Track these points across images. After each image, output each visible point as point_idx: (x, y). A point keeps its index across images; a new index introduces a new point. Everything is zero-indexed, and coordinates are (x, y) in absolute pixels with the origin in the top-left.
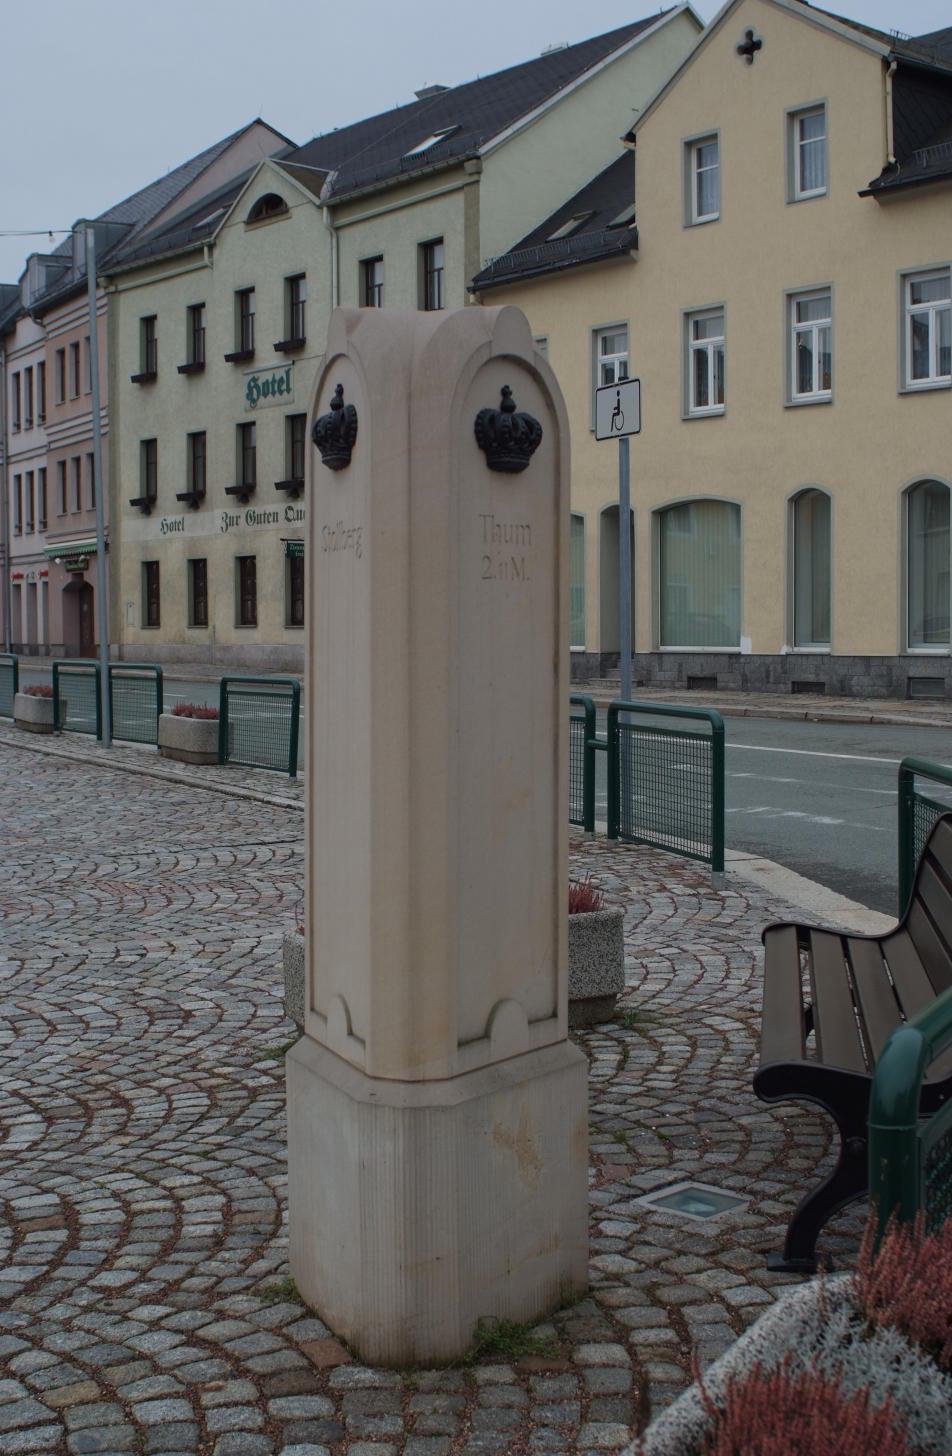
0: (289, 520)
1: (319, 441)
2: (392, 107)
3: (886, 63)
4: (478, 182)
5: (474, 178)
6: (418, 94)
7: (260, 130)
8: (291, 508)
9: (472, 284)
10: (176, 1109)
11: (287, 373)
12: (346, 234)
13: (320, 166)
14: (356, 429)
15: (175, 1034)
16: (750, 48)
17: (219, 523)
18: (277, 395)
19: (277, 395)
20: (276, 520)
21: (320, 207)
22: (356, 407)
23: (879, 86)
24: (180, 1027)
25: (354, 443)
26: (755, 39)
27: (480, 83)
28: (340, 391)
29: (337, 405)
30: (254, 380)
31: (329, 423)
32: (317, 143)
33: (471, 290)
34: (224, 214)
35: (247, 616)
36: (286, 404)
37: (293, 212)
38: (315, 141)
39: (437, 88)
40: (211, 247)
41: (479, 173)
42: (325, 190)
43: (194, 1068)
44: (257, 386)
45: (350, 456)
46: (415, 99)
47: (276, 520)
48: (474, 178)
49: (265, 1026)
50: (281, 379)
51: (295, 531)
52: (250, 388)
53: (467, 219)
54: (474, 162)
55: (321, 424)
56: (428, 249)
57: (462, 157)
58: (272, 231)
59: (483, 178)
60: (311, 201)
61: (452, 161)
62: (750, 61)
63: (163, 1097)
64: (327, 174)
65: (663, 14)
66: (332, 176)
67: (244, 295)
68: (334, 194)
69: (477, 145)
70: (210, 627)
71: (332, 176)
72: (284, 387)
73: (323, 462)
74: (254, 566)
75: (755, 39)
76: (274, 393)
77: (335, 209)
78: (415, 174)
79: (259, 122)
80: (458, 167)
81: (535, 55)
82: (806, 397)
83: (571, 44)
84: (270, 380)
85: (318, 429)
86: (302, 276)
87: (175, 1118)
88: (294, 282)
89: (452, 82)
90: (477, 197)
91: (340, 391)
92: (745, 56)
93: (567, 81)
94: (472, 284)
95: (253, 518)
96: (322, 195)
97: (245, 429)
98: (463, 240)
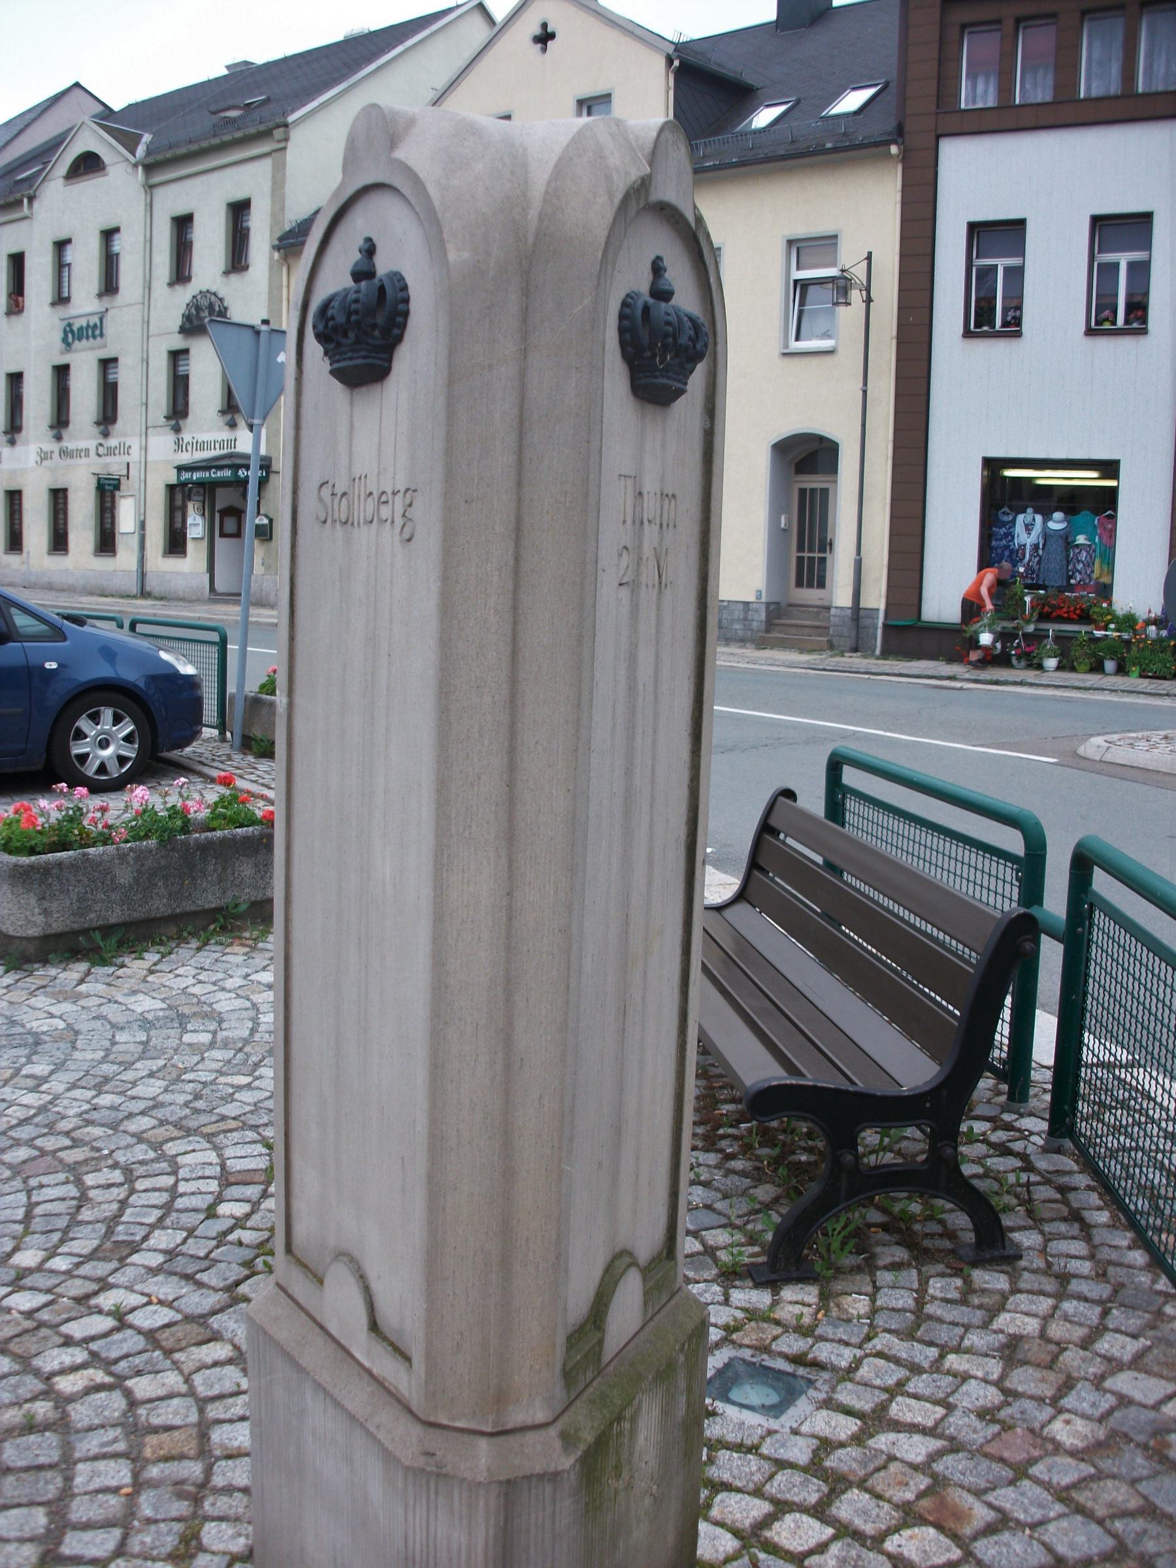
0: (99, 455)
1: (321, 337)
2: (204, 79)
3: (669, 61)
4: (285, 148)
5: (282, 145)
6: (228, 67)
7: (78, 91)
8: (101, 445)
9: (277, 243)
10: (38, 1204)
11: (101, 320)
12: (159, 193)
13: (136, 128)
14: (406, 314)
15: (24, 1072)
16: (545, 38)
17: (33, 457)
18: (91, 339)
19: (91, 339)
20: (87, 455)
21: (135, 166)
22: (405, 275)
23: (662, 80)
24: (29, 1061)
25: (399, 339)
26: (549, 30)
27: (286, 60)
28: (369, 250)
29: (362, 274)
30: (70, 325)
31: (356, 301)
32: (132, 108)
33: (277, 248)
34: (43, 169)
35: (59, 542)
36: (100, 347)
37: (110, 169)
38: (130, 105)
39: (246, 63)
40: (31, 199)
41: (286, 140)
42: (141, 151)
43: (51, 1127)
44: (72, 332)
45: (390, 360)
46: (226, 72)
47: (87, 455)
48: (282, 145)
49: (128, 1058)
50: (95, 326)
51: (107, 465)
52: (65, 332)
53: (274, 182)
54: (281, 130)
55: (335, 304)
56: (239, 210)
57: (271, 124)
58: (89, 186)
59: (290, 145)
60: (127, 160)
61: (262, 128)
62: (544, 50)
63: (17, 1183)
64: (141, 136)
65: (458, 6)
66: (147, 138)
67: (61, 246)
68: (149, 153)
69: (285, 114)
70: (25, 554)
71: (147, 138)
72: (97, 332)
73: (332, 372)
74: (66, 498)
75: (549, 30)
76: (87, 338)
77: (150, 168)
78: (227, 138)
79: (77, 85)
80: (266, 134)
81: (338, 37)
82: (803, 345)
83: (372, 29)
84: (85, 325)
85: (330, 312)
86: (117, 230)
87: (37, 1224)
88: (108, 235)
89: (259, 59)
90: (284, 164)
91: (369, 250)
92: (539, 45)
93: (369, 60)
94: (277, 243)
95: (64, 453)
96: (138, 155)
97: (62, 372)
98: (269, 202)
